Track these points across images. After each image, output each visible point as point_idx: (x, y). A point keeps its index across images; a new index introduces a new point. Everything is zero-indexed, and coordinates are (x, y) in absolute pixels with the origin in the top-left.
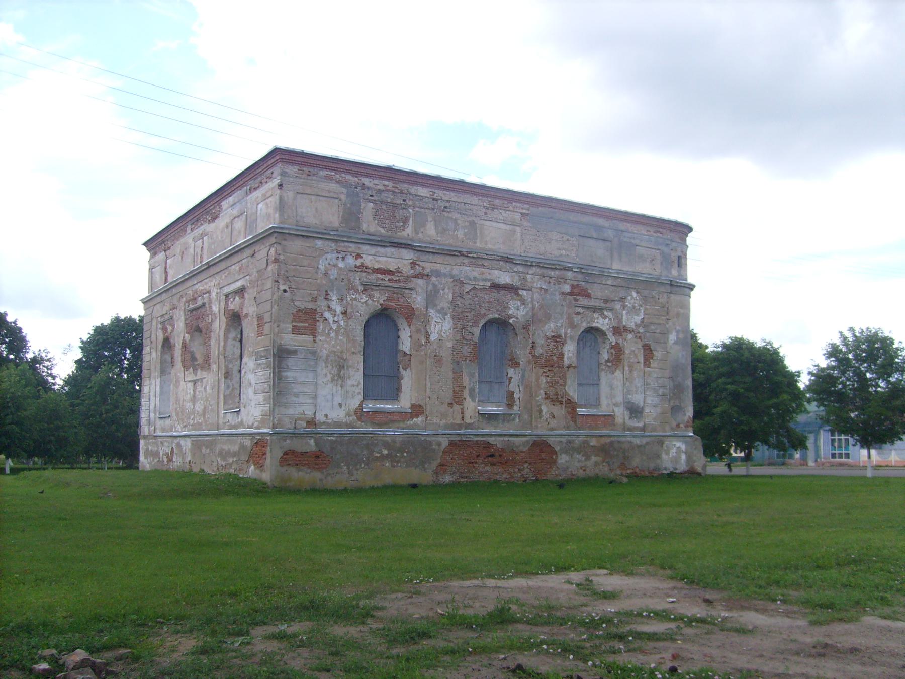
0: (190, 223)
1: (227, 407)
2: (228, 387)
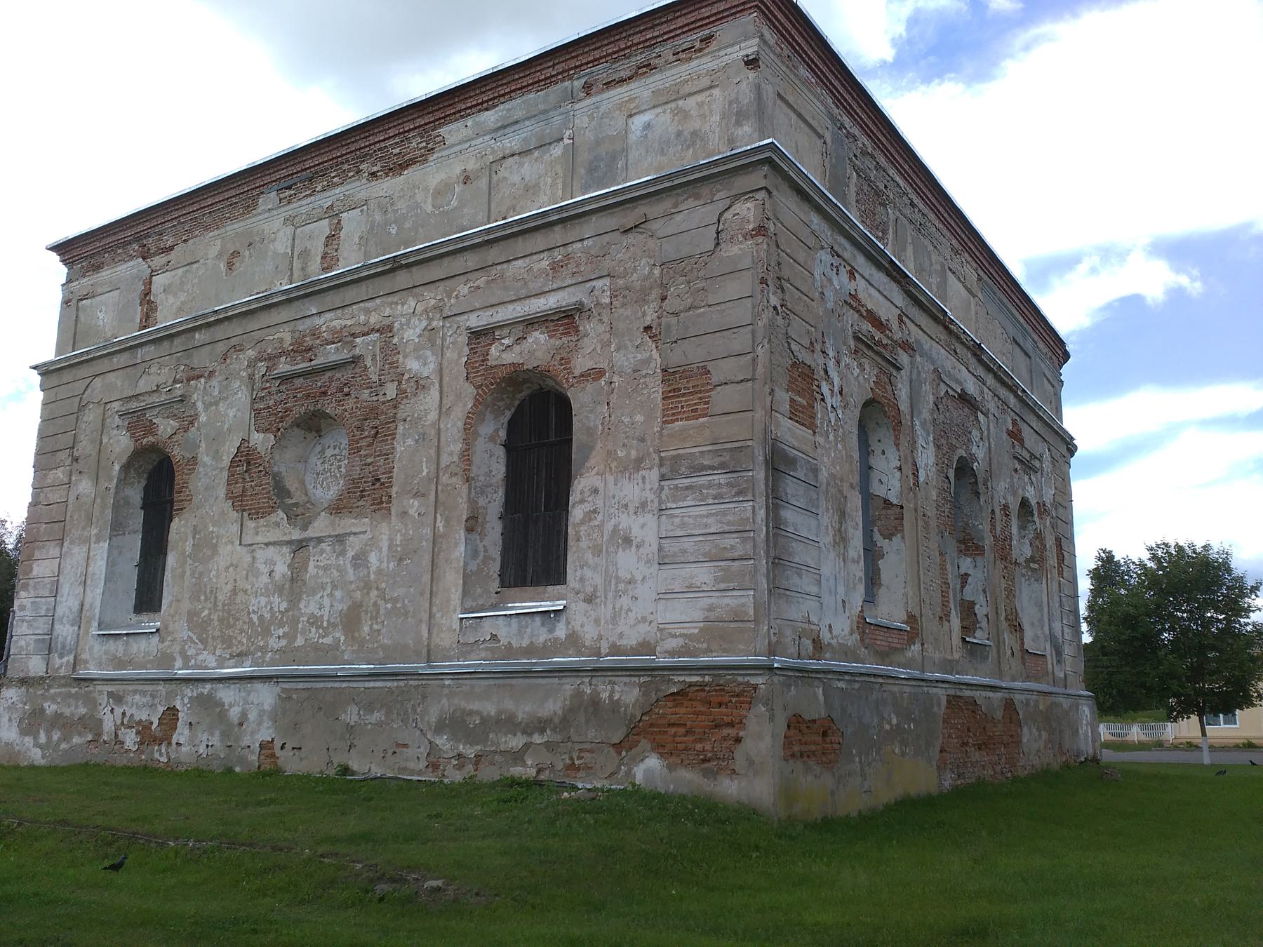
0: (275, 186)
1: (469, 604)
2: (475, 553)
